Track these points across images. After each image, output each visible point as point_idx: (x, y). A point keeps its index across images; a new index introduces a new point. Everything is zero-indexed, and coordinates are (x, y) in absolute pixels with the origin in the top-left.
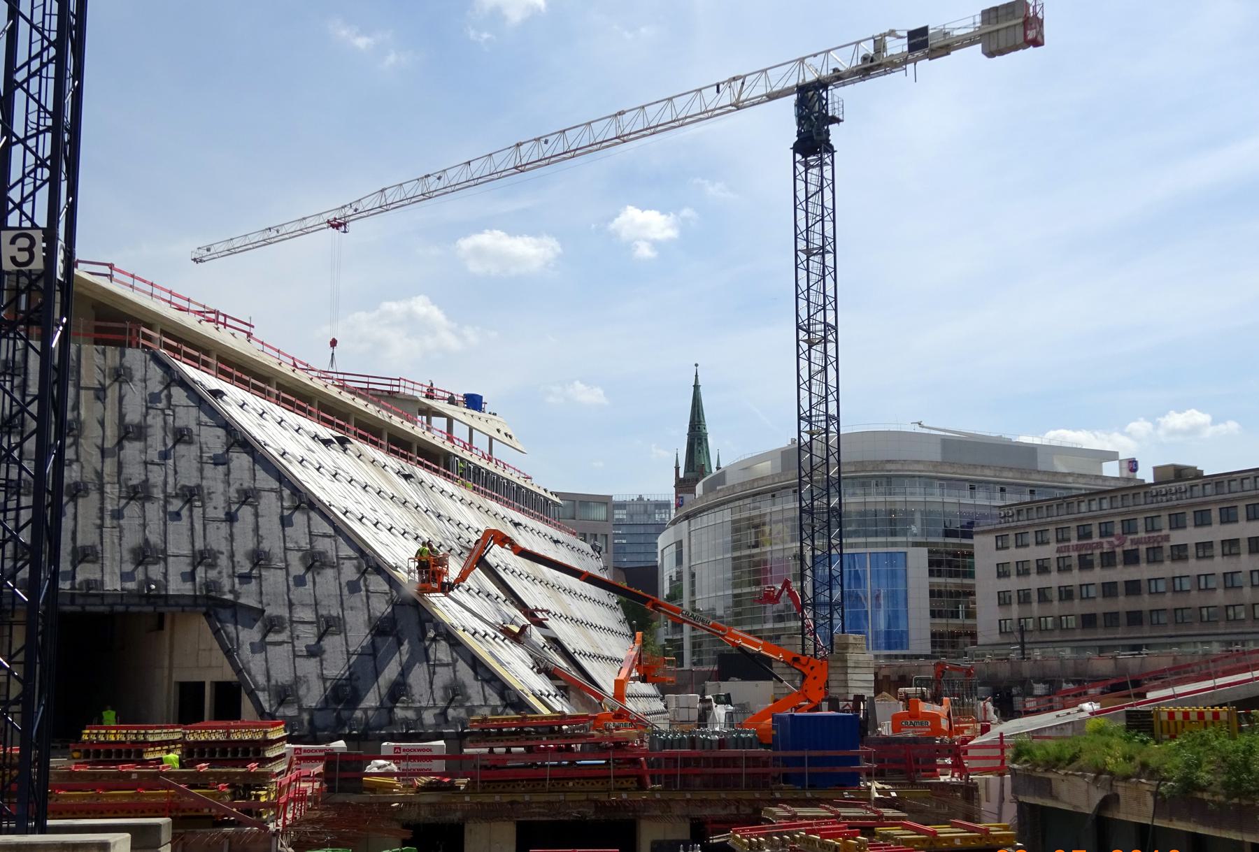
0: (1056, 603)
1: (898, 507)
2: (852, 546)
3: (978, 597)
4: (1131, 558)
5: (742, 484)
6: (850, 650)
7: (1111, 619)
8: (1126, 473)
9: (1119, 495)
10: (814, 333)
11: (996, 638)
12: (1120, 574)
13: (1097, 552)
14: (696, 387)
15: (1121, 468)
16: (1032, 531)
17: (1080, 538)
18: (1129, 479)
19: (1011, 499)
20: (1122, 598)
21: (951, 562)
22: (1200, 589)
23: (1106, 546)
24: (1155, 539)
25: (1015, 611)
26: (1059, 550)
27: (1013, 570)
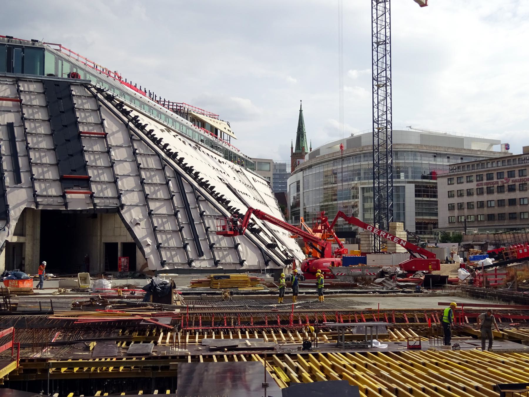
0: (476, 209)
1: (401, 165)
2: (369, 183)
3: (439, 206)
4: (512, 189)
5: (328, 155)
6: (397, 230)
7: (502, 217)
8: (504, 150)
9: (506, 160)
10: (381, 81)
11: (447, 225)
12: (506, 196)
13: (496, 186)
14: (301, 111)
15: (502, 148)
16: (465, 176)
17: (487, 180)
18: (505, 153)
19: (453, 162)
20: (507, 207)
21: (426, 191)
22: (520, 205)
23: (500, 183)
24: (523, 180)
25: (456, 213)
26: (477, 185)
27: (456, 194)
